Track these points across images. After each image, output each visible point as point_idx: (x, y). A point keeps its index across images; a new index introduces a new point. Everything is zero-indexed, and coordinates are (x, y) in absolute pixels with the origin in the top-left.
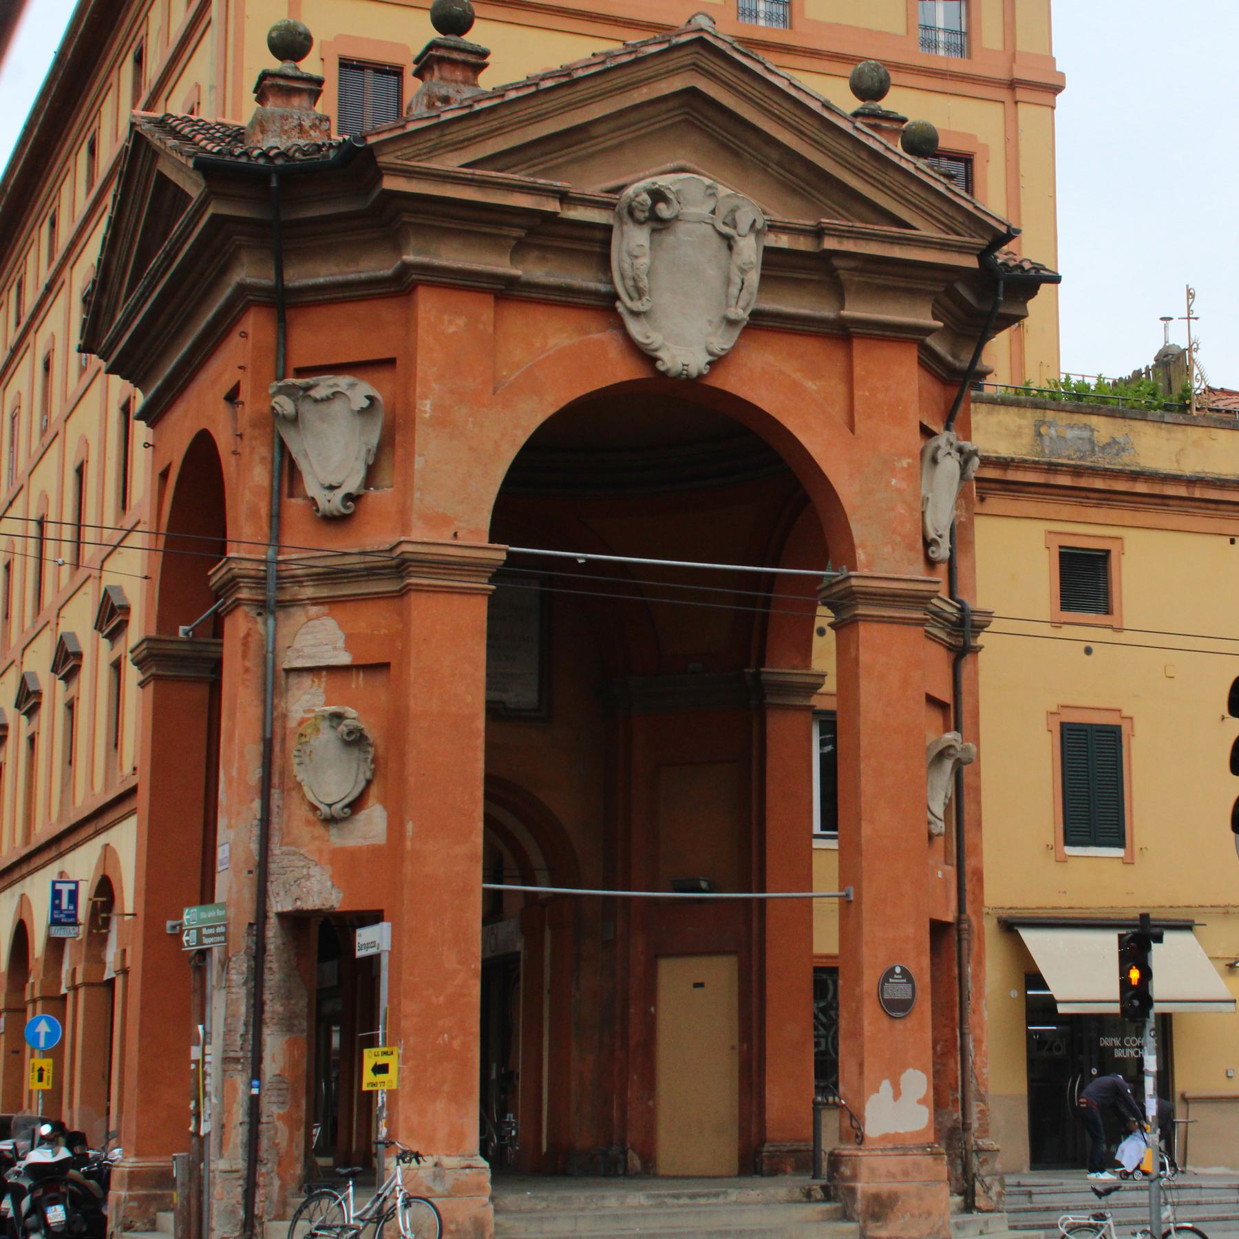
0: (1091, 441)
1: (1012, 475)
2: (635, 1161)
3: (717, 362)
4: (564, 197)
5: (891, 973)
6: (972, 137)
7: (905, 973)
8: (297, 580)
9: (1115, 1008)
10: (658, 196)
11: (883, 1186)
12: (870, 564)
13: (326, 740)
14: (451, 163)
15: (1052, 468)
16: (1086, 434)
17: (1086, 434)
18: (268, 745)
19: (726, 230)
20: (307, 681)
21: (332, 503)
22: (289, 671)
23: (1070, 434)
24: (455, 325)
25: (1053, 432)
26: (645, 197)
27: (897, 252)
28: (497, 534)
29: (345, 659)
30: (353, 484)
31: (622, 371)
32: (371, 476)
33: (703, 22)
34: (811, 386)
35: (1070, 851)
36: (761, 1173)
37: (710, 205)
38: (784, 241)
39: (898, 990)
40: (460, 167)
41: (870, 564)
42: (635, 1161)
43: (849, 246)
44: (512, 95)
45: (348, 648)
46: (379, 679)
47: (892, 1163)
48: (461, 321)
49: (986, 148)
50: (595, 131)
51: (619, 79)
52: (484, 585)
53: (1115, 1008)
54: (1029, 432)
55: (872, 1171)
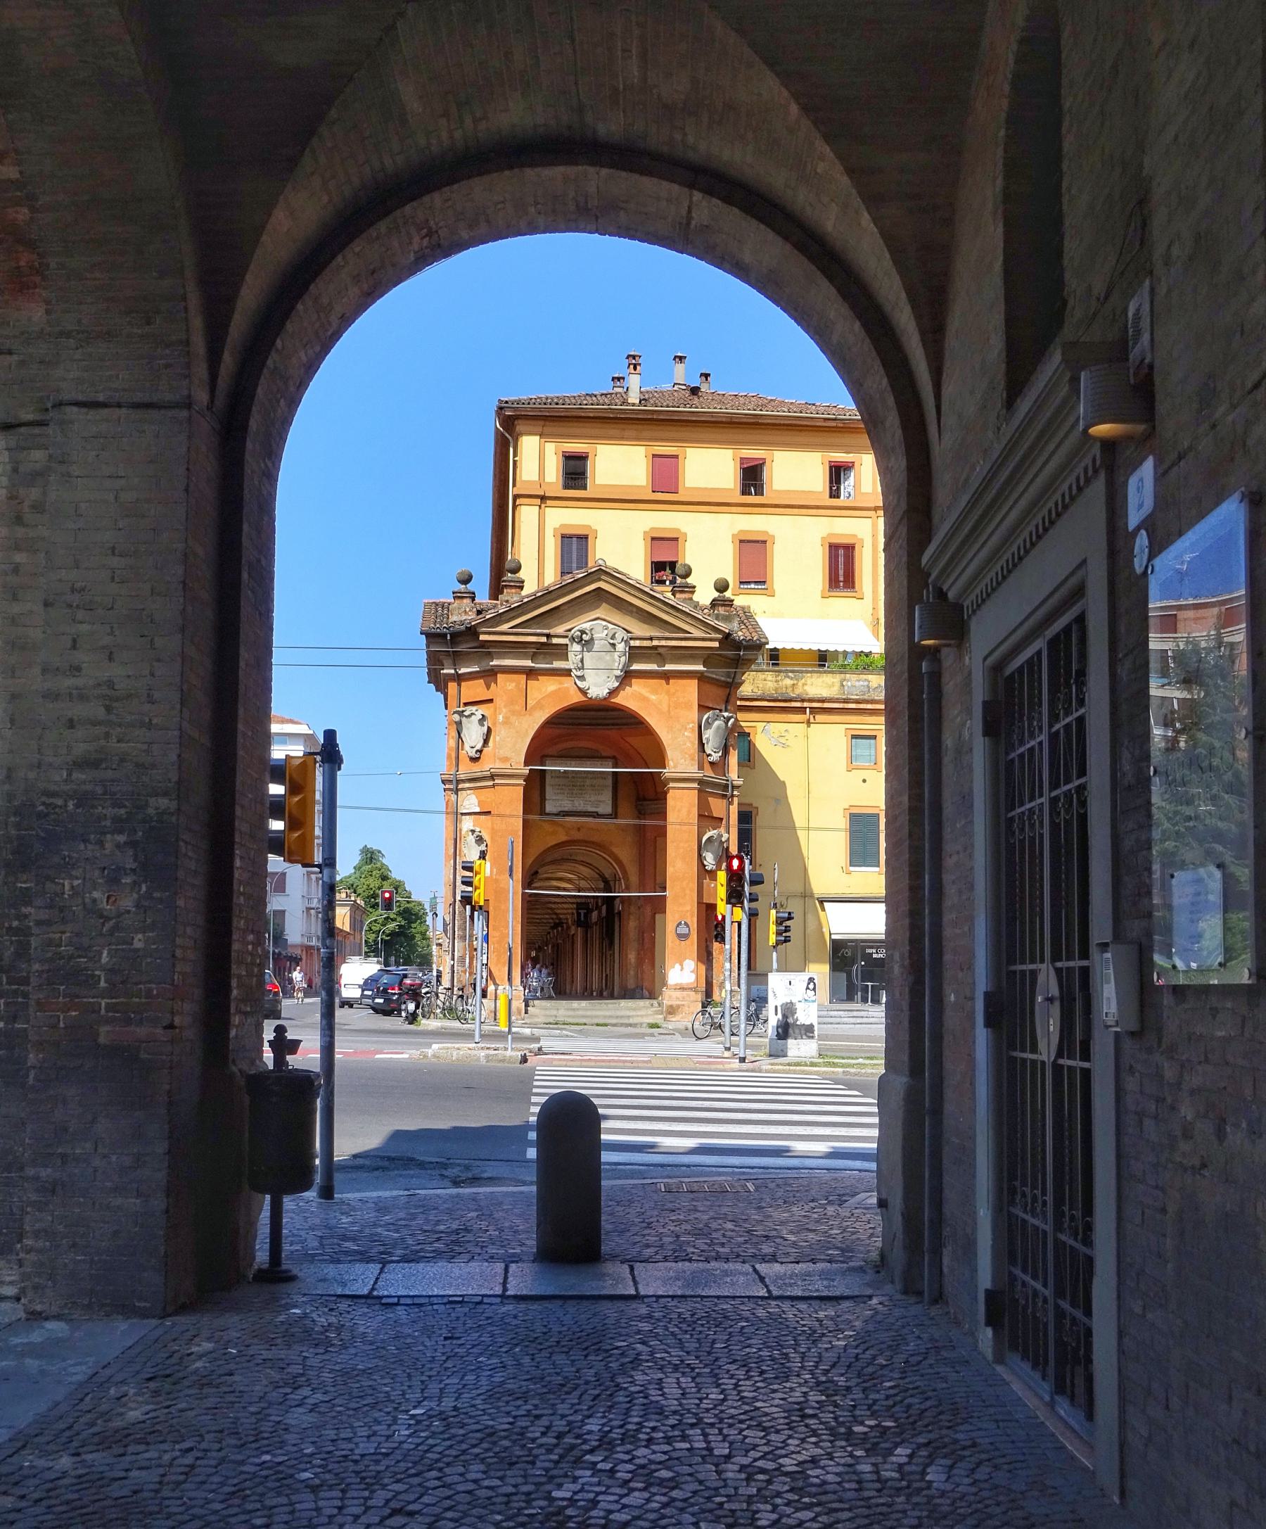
0: (868, 687)
1: (826, 705)
2: (646, 993)
3: (613, 692)
4: (548, 636)
5: (680, 923)
6: (855, 536)
7: (686, 923)
8: (463, 781)
9: (883, 937)
10: (583, 632)
11: (675, 1003)
12: (675, 767)
13: (471, 839)
14: (505, 627)
15: (846, 701)
16: (866, 683)
17: (866, 683)
18: (456, 840)
19: (612, 641)
20: (468, 817)
21: (473, 753)
22: (462, 814)
23: (857, 684)
24: (511, 686)
25: (849, 684)
26: (579, 633)
27: (683, 643)
28: (526, 763)
29: (477, 810)
30: (479, 747)
31: (577, 698)
32: (486, 742)
33: (601, 562)
34: (653, 697)
35: (852, 869)
36: (612, 996)
37: (606, 632)
38: (637, 643)
39: (683, 930)
40: (1010, 403)
41: (675, 767)
42: (646, 993)
43: (663, 643)
44: (526, 600)
45: (479, 805)
46: (488, 817)
47: (679, 994)
48: (514, 684)
49: (862, 540)
50: (562, 608)
51: (568, 588)
52: (522, 782)
53: (883, 937)
54: (837, 685)
55: (670, 997)
